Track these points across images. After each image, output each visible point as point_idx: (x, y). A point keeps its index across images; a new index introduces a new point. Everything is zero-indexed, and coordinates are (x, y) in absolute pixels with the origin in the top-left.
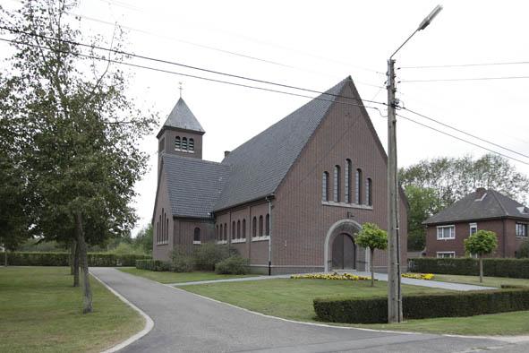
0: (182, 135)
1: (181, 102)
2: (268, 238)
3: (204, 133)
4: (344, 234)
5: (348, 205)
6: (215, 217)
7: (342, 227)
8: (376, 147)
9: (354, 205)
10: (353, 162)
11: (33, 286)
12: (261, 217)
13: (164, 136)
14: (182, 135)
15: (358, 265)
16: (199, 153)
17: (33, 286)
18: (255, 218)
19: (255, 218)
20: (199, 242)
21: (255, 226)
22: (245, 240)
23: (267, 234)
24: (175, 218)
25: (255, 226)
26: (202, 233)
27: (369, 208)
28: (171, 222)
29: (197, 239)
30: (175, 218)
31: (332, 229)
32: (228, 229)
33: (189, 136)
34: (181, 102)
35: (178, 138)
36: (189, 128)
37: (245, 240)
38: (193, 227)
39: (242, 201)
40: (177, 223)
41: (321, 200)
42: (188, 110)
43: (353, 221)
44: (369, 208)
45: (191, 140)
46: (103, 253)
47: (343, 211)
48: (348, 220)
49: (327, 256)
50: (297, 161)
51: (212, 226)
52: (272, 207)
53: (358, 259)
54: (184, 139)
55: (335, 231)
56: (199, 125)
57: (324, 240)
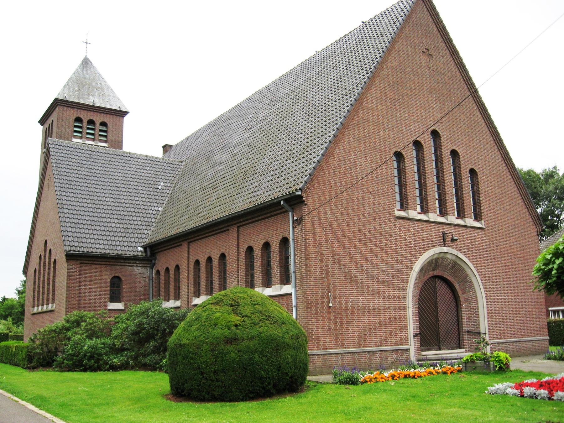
0: (86, 116)
1: (86, 63)
2: (287, 289)
3: (126, 113)
4: (435, 277)
5: (442, 220)
6: (153, 254)
7: (433, 264)
8: (477, 113)
9: (453, 219)
10: (443, 138)
11: (127, 266)
12: (210, 260)
13: (54, 117)
14: (86, 116)
15: (466, 339)
16: (119, 144)
17: (127, 266)
18: (197, 262)
19: (197, 262)
20: (119, 306)
21: (250, 267)
22: (178, 303)
23: (285, 280)
24: (71, 257)
25: (250, 267)
26: (125, 288)
27: (477, 224)
28: (63, 267)
29: (115, 298)
30: (71, 257)
31: (417, 267)
32: (184, 275)
33: (98, 118)
34: (86, 63)
35: (78, 120)
36: (99, 103)
37: (178, 303)
38: (106, 275)
39: (216, 215)
40: (75, 267)
41: (391, 207)
42: (97, 76)
43: (455, 252)
44: (477, 224)
45: (103, 124)
46: (541, 221)
47: (435, 231)
48: (445, 249)
49: (412, 327)
50: (343, 127)
51: (146, 272)
52: (297, 223)
53: (466, 326)
54: (91, 122)
55: (423, 270)
56: (118, 100)
57: (404, 289)
